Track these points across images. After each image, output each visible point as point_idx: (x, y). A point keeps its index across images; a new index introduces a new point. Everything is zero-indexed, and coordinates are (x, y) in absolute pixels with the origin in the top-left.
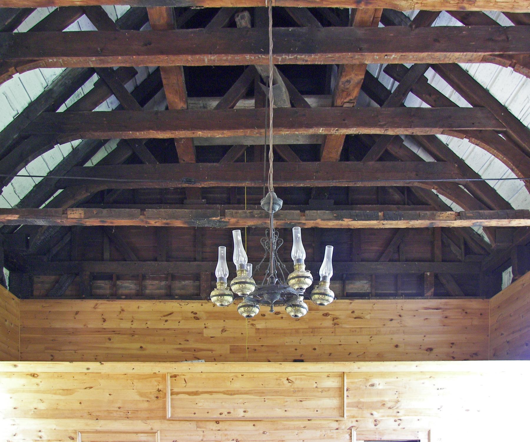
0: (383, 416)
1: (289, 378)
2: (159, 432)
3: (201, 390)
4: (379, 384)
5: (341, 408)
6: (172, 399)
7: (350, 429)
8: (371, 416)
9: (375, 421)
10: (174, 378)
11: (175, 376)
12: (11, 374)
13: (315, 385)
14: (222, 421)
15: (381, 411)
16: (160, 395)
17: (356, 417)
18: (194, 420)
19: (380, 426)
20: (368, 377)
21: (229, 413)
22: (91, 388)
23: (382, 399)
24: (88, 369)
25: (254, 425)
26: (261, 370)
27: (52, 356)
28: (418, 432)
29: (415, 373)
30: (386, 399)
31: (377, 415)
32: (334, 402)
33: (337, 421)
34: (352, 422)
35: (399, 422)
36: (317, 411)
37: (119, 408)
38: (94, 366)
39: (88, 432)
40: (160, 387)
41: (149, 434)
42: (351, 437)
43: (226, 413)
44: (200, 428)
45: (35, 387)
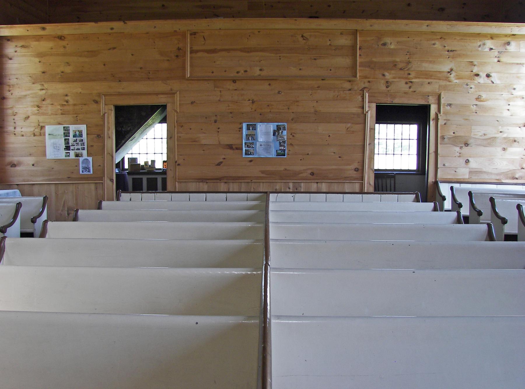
0: (394, 78)
1: (304, 35)
2: (178, 93)
3: (219, 47)
4: (391, 43)
5: (354, 67)
6: (191, 58)
7: (363, 90)
8: (383, 77)
9: (387, 82)
10: (193, 36)
11: (195, 34)
12: (38, 38)
13: (329, 43)
14: (239, 80)
15: (393, 72)
16: (180, 53)
17: (368, 78)
18: (212, 80)
19: (392, 88)
20: (380, 35)
21: (246, 71)
22: (114, 48)
23: (394, 59)
24: (112, 29)
25: (270, 85)
26: (277, 26)
27: (78, 18)
28: (428, 96)
29: (425, 33)
30: (398, 60)
31: (388, 76)
32: (346, 61)
33: (350, 81)
34: (364, 83)
35: (410, 84)
36: (330, 70)
37: (141, 68)
38: (117, 25)
39: (111, 95)
40: (180, 46)
41: (169, 96)
42: (363, 99)
43: (242, 72)
44: (218, 87)
45: (62, 50)
